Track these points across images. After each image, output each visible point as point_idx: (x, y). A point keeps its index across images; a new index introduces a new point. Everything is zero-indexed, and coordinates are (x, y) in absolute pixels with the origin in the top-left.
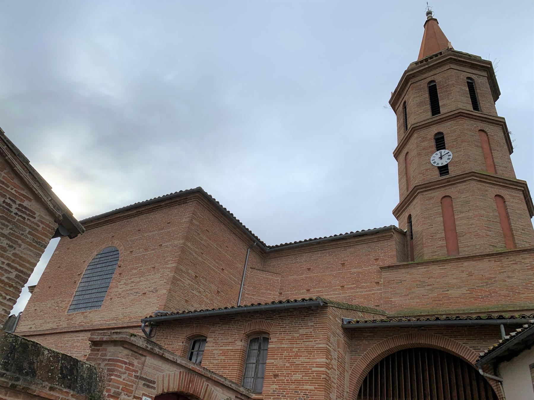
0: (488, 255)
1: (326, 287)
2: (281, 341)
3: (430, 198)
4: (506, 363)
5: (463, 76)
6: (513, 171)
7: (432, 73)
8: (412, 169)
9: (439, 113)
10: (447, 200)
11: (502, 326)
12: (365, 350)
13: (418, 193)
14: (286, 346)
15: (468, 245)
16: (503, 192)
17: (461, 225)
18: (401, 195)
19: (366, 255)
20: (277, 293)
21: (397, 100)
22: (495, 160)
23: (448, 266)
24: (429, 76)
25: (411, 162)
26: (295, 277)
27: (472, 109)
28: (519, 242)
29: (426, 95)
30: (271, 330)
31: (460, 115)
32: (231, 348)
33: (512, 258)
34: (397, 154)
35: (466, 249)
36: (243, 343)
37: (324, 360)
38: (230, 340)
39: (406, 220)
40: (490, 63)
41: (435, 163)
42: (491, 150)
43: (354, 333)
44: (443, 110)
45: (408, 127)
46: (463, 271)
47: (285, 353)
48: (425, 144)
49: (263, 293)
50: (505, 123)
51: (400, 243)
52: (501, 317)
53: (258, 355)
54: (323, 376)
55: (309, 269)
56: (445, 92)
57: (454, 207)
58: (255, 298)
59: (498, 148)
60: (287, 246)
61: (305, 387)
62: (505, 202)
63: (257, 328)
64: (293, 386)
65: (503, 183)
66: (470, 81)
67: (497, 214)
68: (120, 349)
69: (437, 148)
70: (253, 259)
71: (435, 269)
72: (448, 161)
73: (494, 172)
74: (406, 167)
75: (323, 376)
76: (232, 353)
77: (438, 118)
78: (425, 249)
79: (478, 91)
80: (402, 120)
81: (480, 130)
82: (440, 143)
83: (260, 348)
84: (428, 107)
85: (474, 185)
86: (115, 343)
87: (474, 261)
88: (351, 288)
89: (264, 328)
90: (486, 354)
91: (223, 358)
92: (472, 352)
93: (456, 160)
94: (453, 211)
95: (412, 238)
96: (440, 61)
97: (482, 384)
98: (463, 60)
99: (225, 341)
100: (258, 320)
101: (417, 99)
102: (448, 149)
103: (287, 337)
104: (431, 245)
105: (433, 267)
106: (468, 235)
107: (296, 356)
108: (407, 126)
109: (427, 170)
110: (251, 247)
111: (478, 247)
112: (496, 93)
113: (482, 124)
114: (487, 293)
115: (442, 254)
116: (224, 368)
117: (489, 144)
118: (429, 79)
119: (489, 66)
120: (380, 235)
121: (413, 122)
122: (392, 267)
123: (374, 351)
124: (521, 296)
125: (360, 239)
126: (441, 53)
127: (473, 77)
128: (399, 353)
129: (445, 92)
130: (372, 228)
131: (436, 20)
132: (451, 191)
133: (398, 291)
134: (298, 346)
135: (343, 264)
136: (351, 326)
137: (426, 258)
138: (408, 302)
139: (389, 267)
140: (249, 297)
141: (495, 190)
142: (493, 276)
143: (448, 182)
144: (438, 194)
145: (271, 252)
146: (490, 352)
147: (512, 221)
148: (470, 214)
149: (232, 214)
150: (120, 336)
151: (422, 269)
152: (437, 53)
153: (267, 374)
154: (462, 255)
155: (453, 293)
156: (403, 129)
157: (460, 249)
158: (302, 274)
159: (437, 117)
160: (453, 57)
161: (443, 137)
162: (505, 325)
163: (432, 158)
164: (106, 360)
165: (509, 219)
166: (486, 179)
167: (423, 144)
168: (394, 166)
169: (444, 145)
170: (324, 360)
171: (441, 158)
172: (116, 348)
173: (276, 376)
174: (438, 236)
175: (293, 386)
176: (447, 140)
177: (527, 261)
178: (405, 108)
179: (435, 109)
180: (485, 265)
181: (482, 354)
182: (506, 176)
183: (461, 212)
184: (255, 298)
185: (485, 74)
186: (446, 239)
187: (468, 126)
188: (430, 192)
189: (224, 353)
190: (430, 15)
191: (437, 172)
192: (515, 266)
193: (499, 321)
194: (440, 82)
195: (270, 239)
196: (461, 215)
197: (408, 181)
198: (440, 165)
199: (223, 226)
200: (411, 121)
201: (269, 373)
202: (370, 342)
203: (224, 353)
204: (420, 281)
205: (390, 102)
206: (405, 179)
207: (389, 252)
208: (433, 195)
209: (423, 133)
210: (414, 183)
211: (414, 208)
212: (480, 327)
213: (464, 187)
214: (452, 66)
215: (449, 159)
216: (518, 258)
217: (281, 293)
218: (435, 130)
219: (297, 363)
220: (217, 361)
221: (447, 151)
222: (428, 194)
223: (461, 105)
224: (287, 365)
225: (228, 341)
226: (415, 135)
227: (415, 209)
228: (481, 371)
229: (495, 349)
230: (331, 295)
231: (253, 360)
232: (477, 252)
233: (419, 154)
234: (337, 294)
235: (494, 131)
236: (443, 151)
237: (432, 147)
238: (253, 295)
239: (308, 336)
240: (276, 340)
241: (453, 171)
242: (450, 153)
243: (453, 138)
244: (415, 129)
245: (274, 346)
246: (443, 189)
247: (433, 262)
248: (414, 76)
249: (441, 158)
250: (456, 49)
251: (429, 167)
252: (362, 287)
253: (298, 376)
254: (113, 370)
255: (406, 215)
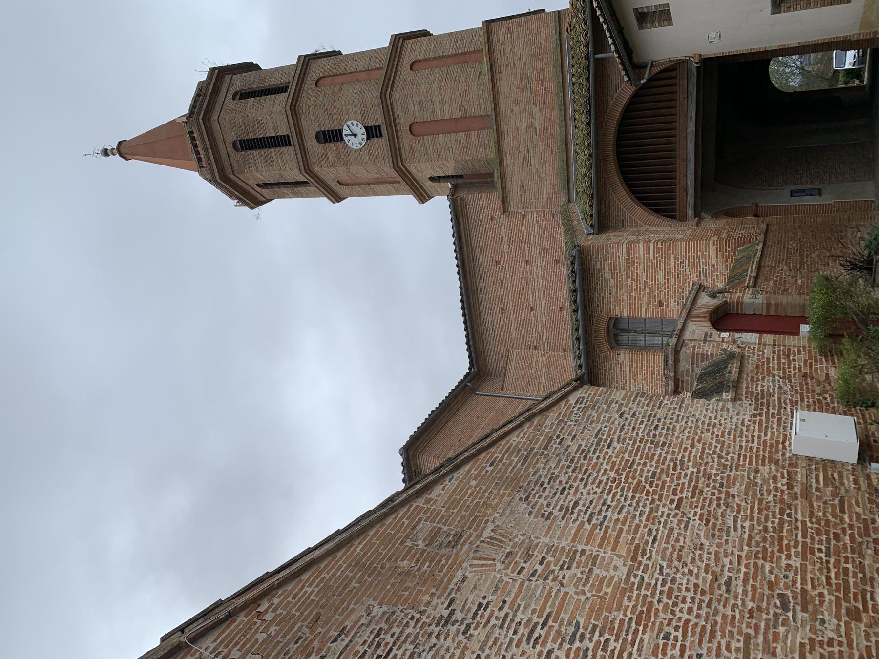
0: (493, 81)
1: (527, 284)
2: (619, 302)
3: (412, 149)
4: (634, 55)
5: (230, 104)
6: (363, 53)
7: (221, 145)
8: (363, 173)
9: (288, 136)
10: (416, 128)
11: (596, 56)
12: (621, 210)
13: (404, 167)
14: (625, 294)
15: (479, 104)
16: (407, 61)
17: (450, 111)
18: (398, 192)
19: (486, 232)
20: (535, 352)
21: (251, 198)
22: (360, 69)
23: (505, 128)
24: (226, 149)
25: (354, 176)
26: (513, 328)
27: (287, 94)
28: (473, 46)
29: (256, 154)
30: (605, 315)
31: (294, 109)
32: (628, 368)
33: (497, 54)
34: (336, 198)
35: (483, 107)
36: (622, 352)
37: (641, 245)
38: (618, 370)
39: (435, 184)
40: (212, 70)
41: (360, 144)
42: (346, 74)
43: (603, 222)
44: (283, 131)
45: (303, 179)
46: (512, 111)
47: (634, 294)
48: (331, 156)
49: (536, 372)
50: (306, 56)
51: (468, 188)
52: (587, 57)
53: (635, 332)
54: (659, 245)
55: (503, 309)
56: (251, 132)
57: (426, 119)
58: (543, 382)
59: (343, 66)
60: (471, 341)
61: (672, 266)
62: (420, 61)
63: (603, 334)
64: (672, 280)
65: (394, 61)
66: (238, 97)
67: (436, 70)
68: (682, 355)
69: (338, 140)
70: (490, 388)
71: (509, 143)
72: (360, 126)
73: (380, 72)
74: (359, 184)
75: (659, 245)
76: (635, 365)
77: (295, 137)
78: (480, 156)
79: (255, 86)
80: (285, 190)
81: (316, 85)
82: (333, 136)
83: (625, 331)
84: (274, 151)
85: (398, 94)
86: (676, 361)
87: (499, 98)
88: (530, 250)
89: (603, 326)
90: (627, 74)
91: (640, 377)
92: (622, 90)
93: (360, 115)
94: (431, 121)
95: (461, 176)
96: (205, 133)
97: (656, 83)
98: (206, 104)
99: (619, 377)
100: (594, 335)
101: (258, 168)
102: (342, 126)
103: (615, 295)
104: (477, 149)
105: (505, 146)
106: (465, 103)
107: (636, 280)
108: (302, 182)
109: (370, 154)
110: (473, 391)
111: (481, 92)
112: (250, 67)
113: (308, 83)
114: (540, 84)
115: (488, 137)
116: (652, 373)
117: (337, 75)
118: (230, 149)
119: (217, 71)
120: (460, 213)
121: (296, 172)
122: (503, 197)
123: (622, 200)
124: (543, 46)
125: (464, 240)
126: (191, 133)
127: (232, 92)
128: (622, 173)
129: (251, 132)
130: (451, 224)
131: (120, 143)
132: (404, 122)
133: (535, 190)
134: (625, 279)
135: (497, 263)
136: (596, 226)
137: (493, 155)
138: (548, 178)
139: (503, 202)
140: (542, 389)
141: (404, 72)
142: (518, 76)
143: (391, 125)
144: (407, 140)
145: (478, 365)
146: (625, 69)
147: (446, 54)
148: (437, 100)
149: (432, 411)
150: (670, 355)
151: (508, 160)
152: (188, 137)
153: (658, 316)
154: (490, 111)
155: (538, 122)
156: (302, 189)
157: (483, 114)
158: (509, 320)
159: (294, 139)
160: (201, 116)
161: (324, 132)
162: (595, 53)
163: (354, 147)
164: (692, 367)
165: (443, 57)
166: (389, 80)
167: (331, 159)
168: (352, 203)
169: (336, 131)
170: (641, 245)
171: (355, 135)
172: (681, 359)
173: (660, 304)
174: (464, 141)
175: (672, 280)
176: (328, 125)
177: (501, 37)
178: (266, 185)
179: (281, 141)
180: (504, 85)
181: (626, 79)
182: (385, 59)
183: (434, 111)
184: (543, 382)
185: (228, 78)
186: (468, 130)
187: (309, 99)
188: (403, 151)
189: (634, 376)
190: (109, 152)
191: (375, 141)
192: (508, 51)
193: (591, 59)
194: (237, 134)
195: (460, 367)
196: (438, 112)
197: (379, 182)
198: (365, 136)
199: (450, 424)
200: (294, 174)
201: (657, 313)
202: (611, 204)
203: (634, 376)
204: (523, 163)
205: (252, 208)
206: (376, 186)
207: (484, 204)
208: (407, 147)
209: (314, 158)
210: (388, 171)
211: (422, 172)
212: (599, 76)
213: (399, 107)
214: (215, 117)
215: (357, 125)
216: (498, 47)
217: (535, 348)
218: (311, 143)
219: (645, 278)
220: (645, 385)
221: (345, 127)
222: (406, 153)
223: (278, 108)
224: (647, 290)
225: (619, 373)
226: (316, 169)
227: (422, 170)
228: (642, 82)
229: (622, 63)
230: (538, 277)
231: (641, 339)
232: (488, 94)
233: (346, 164)
234: (537, 269)
235: (316, 70)
236: (344, 133)
237: (337, 148)
238: (539, 384)
239: (613, 267)
240: (618, 308)
241: (377, 119)
242: (349, 123)
243: (327, 120)
244: (307, 169)
245: (625, 310)
246: (400, 133)
247: (499, 146)
248: (221, 170)
249: (355, 135)
250: (186, 110)
251: (366, 151)
252: (529, 237)
253: (660, 275)
254: (703, 355)
255: (428, 185)
